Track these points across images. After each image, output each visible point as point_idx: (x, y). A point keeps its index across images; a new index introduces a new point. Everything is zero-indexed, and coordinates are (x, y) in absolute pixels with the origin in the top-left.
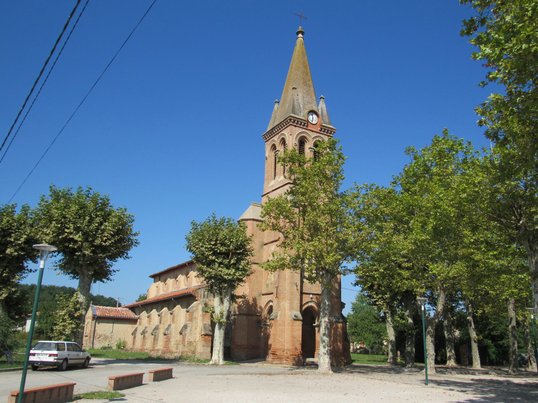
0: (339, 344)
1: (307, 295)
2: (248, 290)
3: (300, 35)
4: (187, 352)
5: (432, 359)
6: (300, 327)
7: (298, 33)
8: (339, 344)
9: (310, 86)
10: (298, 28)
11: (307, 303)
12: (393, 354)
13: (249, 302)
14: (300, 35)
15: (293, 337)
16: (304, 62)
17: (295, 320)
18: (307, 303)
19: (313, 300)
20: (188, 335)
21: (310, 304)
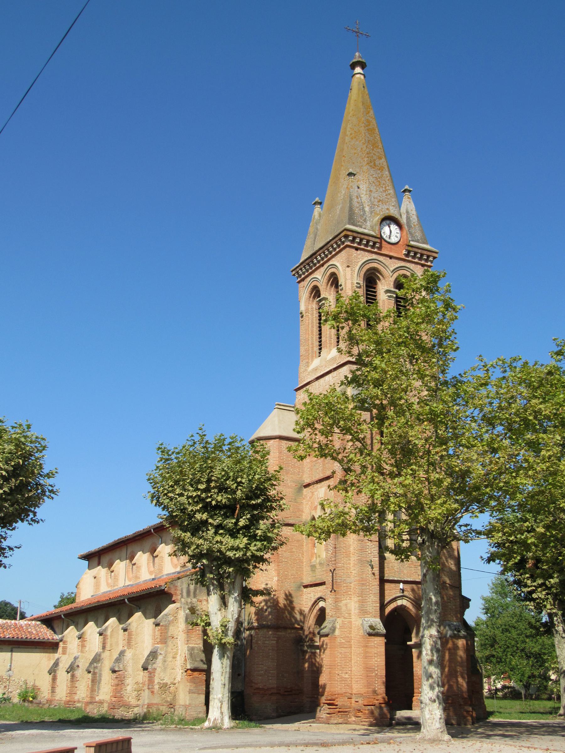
0: (460, 680)
1: (393, 585)
2: (276, 579)
3: (358, 70)
8: (460, 680)
10: (354, 56)
11: (394, 600)
13: (278, 602)
14: (358, 70)
15: (368, 669)
16: (368, 121)
17: (370, 635)
18: (394, 600)
21: (399, 602)
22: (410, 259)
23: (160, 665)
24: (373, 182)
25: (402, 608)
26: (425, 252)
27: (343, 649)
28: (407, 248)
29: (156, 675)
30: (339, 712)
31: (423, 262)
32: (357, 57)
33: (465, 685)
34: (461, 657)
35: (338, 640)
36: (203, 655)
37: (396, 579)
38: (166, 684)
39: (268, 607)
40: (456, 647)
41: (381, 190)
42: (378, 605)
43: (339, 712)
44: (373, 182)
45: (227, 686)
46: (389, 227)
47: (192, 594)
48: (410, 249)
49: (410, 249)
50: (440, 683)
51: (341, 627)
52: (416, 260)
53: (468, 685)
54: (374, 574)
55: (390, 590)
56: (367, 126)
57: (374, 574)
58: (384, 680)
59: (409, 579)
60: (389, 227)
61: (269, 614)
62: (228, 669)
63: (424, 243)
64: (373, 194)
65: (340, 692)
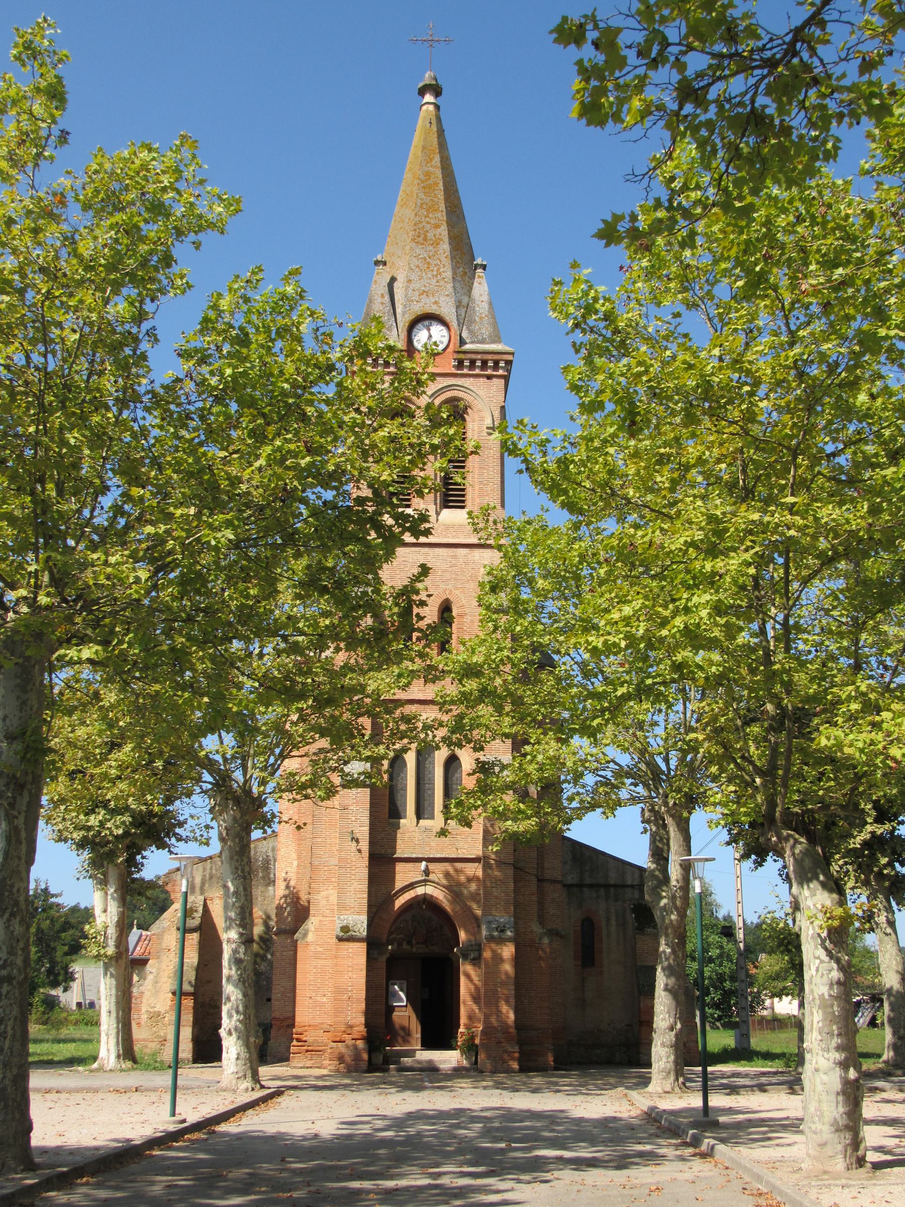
0: (504, 1008)
1: (410, 865)
2: (295, 863)
3: (429, 98)
4: (144, 1040)
5: (663, 1045)
6: (362, 960)
7: (422, 92)
8: (504, 1008)
9: (436, 243)
10: (422, 77)
11: (411, 886)
12: (894, 1034)
13: (298, 898)
14: (429, 98)
15: (339, 991)
16: (428, 174)
17: (340, 939)
18: (411, 886)
19: (432, 877)
20: (147, 994)
21: (420, 891)
22: (465, 371)
23: (150, 987)
24: (418, 266)
25: (427, 902)
26: (489, 357)
27: (320, 961)
28: (456, 356)
29: (144, 1000)
30: (307, 1051)
31: (489, 372)
32: (427, 78)
33: (512, 1016)
34: (507, 973)
35: (312, 948)
36: (194, 973)
37: (414, 856)
38: (158, 1014)
39: (288, 905)
40: (498, 958)
41: (429, 276)
42: (366, 896)
43: (307, 1051)
44: (418, 266)
45: (114, 1014)
46: (429, 330)
47: (198, 889)
48: (462, 356)
49: (462, 356)
50: (241, 1008)
51: (316, 930)
52: (477, 371)
53: (516, 1013)
54: (360, 851)
55: (405, 873)
56: (423, 182)
57: (360, 851)
58: (363, 1006)
59: (438, 856)
60: (429, 330)
61: (289, 914)
62: (114, 991)
63: (493, 342)
64: (412, 286)
65: (312, 1022)
